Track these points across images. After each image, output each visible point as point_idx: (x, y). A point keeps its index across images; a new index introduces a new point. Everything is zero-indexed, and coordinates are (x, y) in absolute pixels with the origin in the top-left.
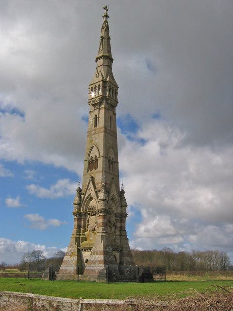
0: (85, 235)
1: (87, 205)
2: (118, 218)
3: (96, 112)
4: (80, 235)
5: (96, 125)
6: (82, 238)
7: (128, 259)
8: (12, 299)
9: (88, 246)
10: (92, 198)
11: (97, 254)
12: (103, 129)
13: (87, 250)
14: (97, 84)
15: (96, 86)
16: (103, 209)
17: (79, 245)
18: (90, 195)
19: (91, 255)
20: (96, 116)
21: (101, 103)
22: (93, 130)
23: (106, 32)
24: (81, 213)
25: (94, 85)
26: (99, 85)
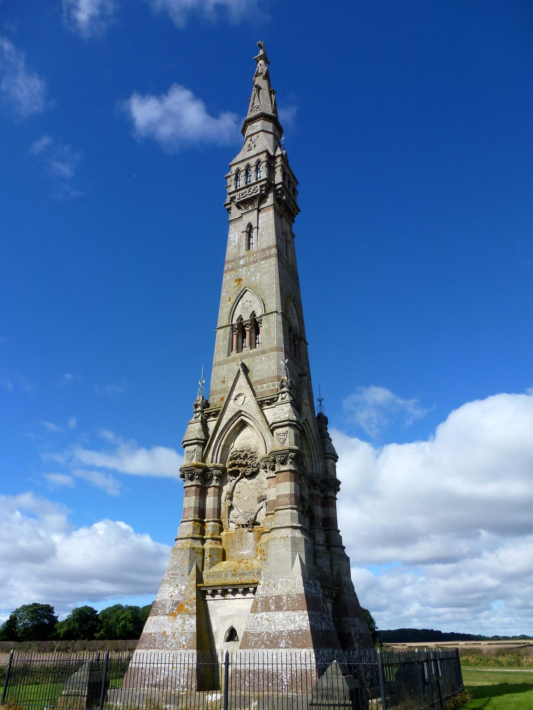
0: (220, 540)
1: (226, 447)
2: (317, 492)
3: (251, 217)
4: (203, 541)
5: (249, 245)
6: (211, 550)
7: (181, 639)
8: (244, 463)
9: (237, 580)
10: (243, 425)
11: (279, 608)
12: (274, 251)
13: (235, 592)
14: (253, 162)
15: (248, 167)
16: (291, 450)
17: (199, 579)
18: (239, 413)
19: (254, 610)
20: (250, 226)
21: (262, 198)
22: (244, 257)
23: (235, 181)
24: (206, 470)
25: (245, 163)
26: (259, 162)
